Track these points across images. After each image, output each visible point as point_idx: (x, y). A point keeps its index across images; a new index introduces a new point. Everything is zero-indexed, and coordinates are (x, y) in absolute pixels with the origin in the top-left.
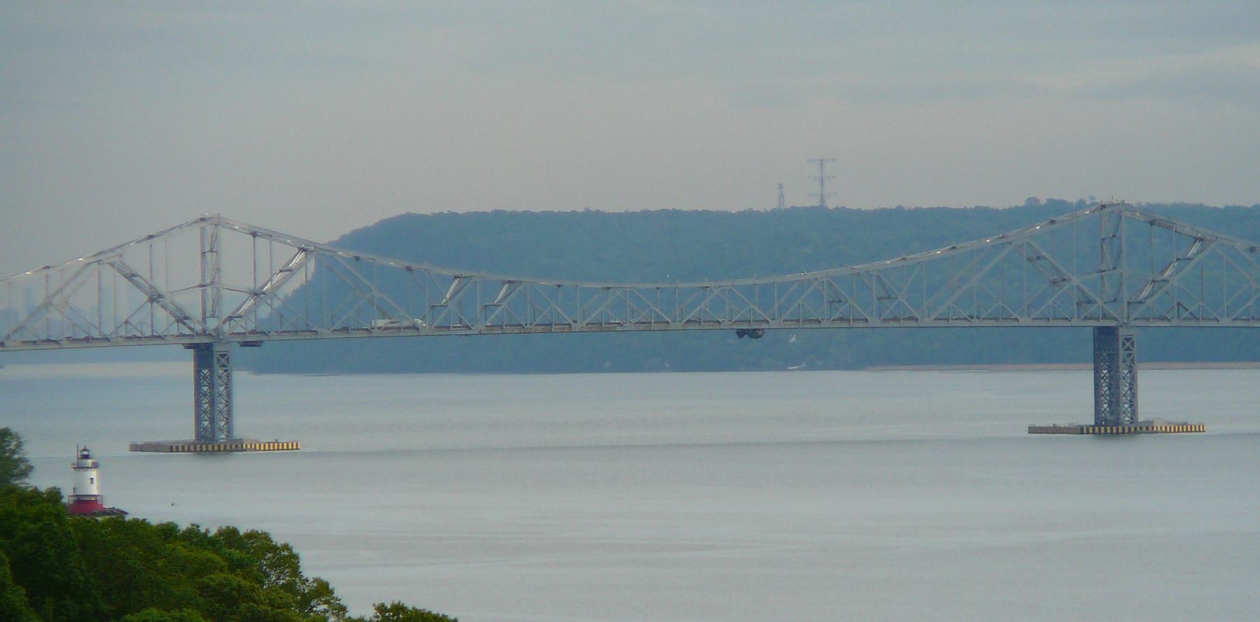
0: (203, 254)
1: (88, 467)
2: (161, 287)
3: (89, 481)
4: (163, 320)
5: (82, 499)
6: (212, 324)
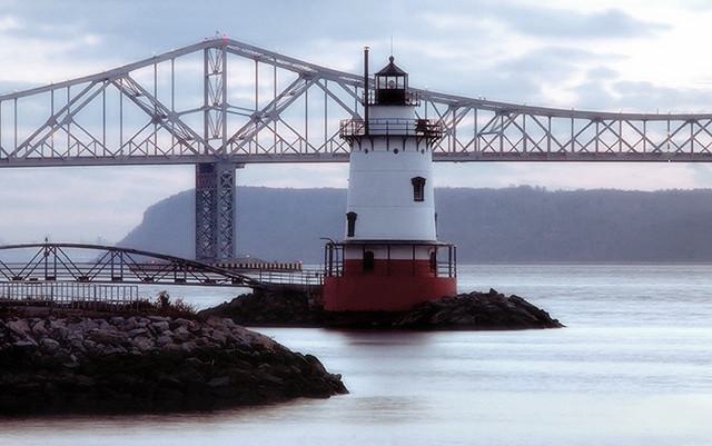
0: (207, 77)
1: (404, 138)
2: (165, 100)
3: (411, 188)
4: (165, 142)
5: (380, 255)
6: (216, 145)
